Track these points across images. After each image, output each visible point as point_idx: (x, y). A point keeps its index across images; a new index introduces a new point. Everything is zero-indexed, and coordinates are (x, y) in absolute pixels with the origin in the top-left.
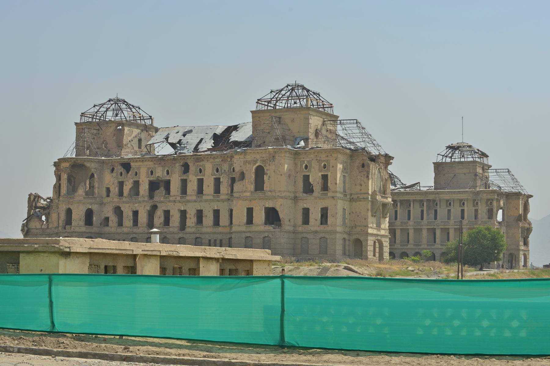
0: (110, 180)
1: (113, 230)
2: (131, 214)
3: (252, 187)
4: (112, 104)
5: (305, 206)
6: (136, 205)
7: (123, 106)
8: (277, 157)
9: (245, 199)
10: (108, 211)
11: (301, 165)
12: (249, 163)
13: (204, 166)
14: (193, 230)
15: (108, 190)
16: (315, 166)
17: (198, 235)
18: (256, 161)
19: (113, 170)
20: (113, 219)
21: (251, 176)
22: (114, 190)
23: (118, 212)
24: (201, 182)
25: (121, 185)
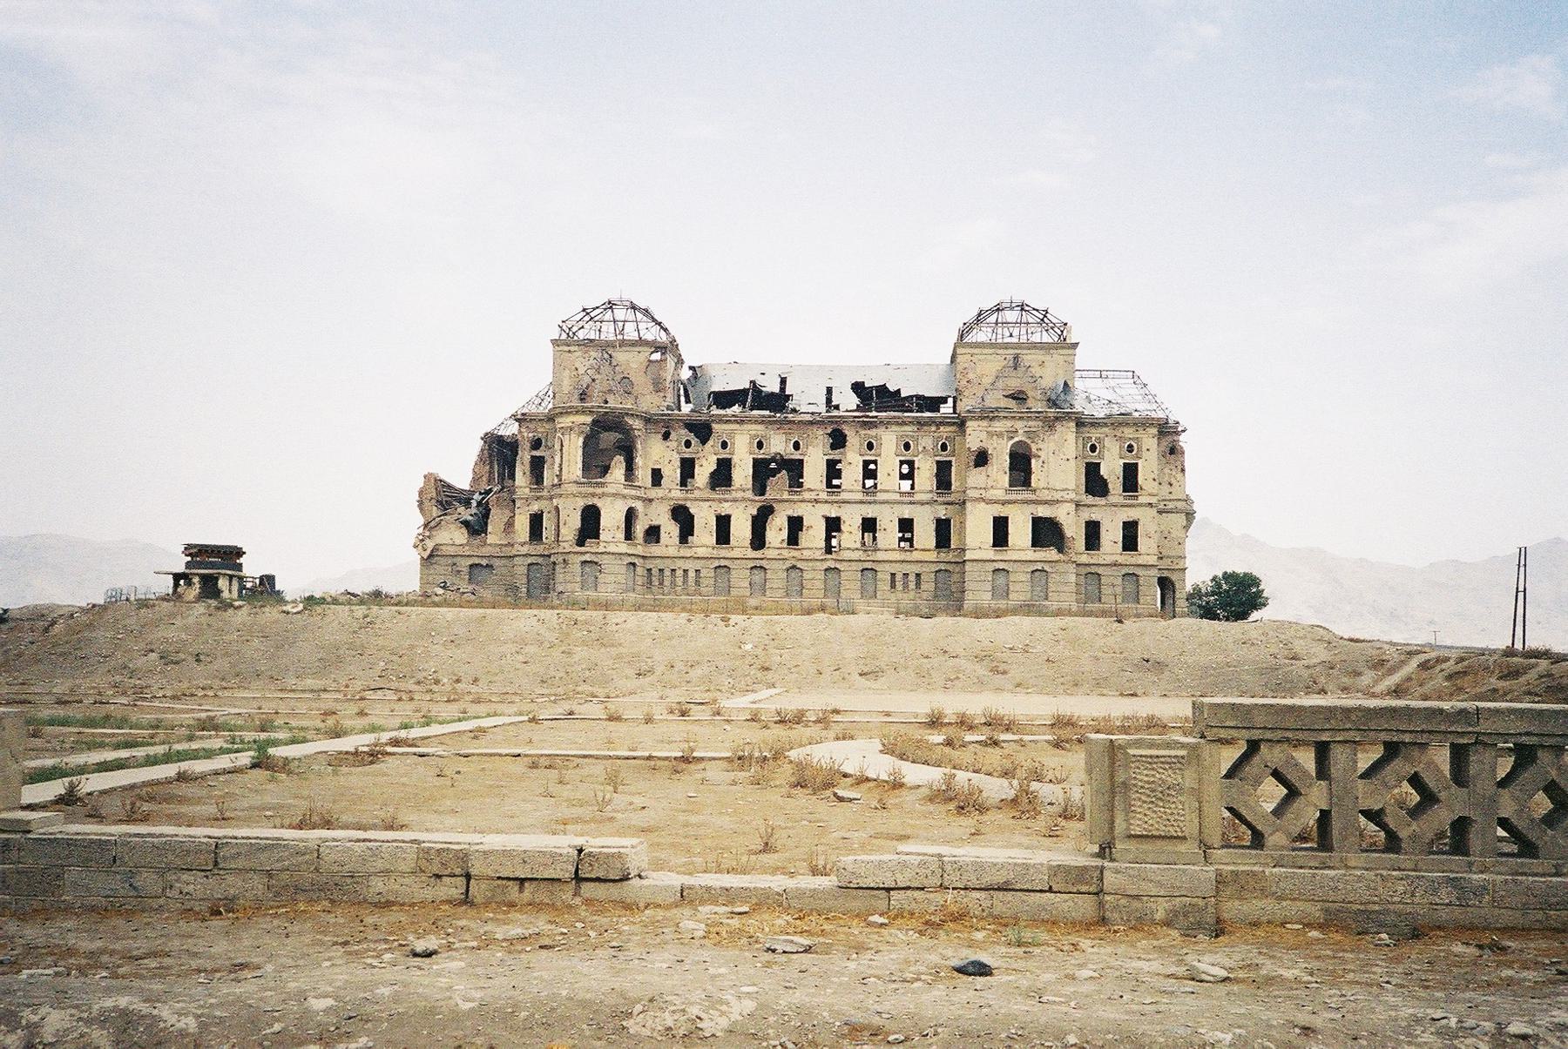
1: (672, 551)
5: (1094, 517)
12: (1000, 435)
19: (666, 436)
20: (670, 530)
22: (672, 473)
23: (683, 518)
25: (688, 468)
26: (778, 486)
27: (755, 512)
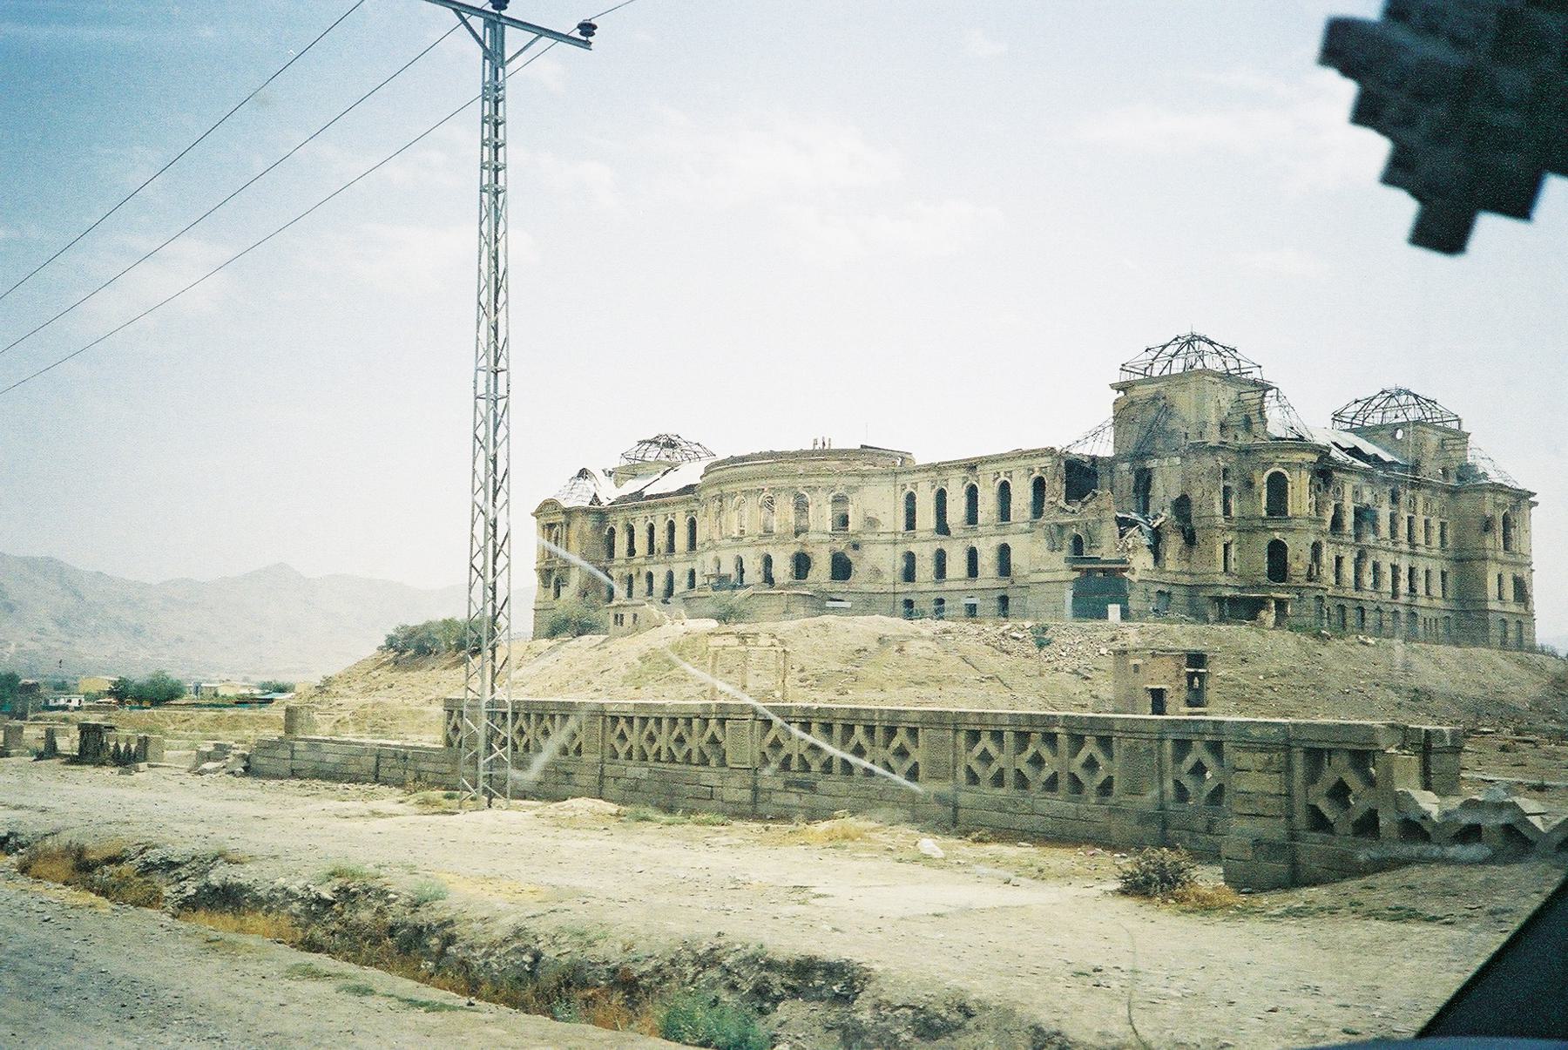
26: (1366, 526)
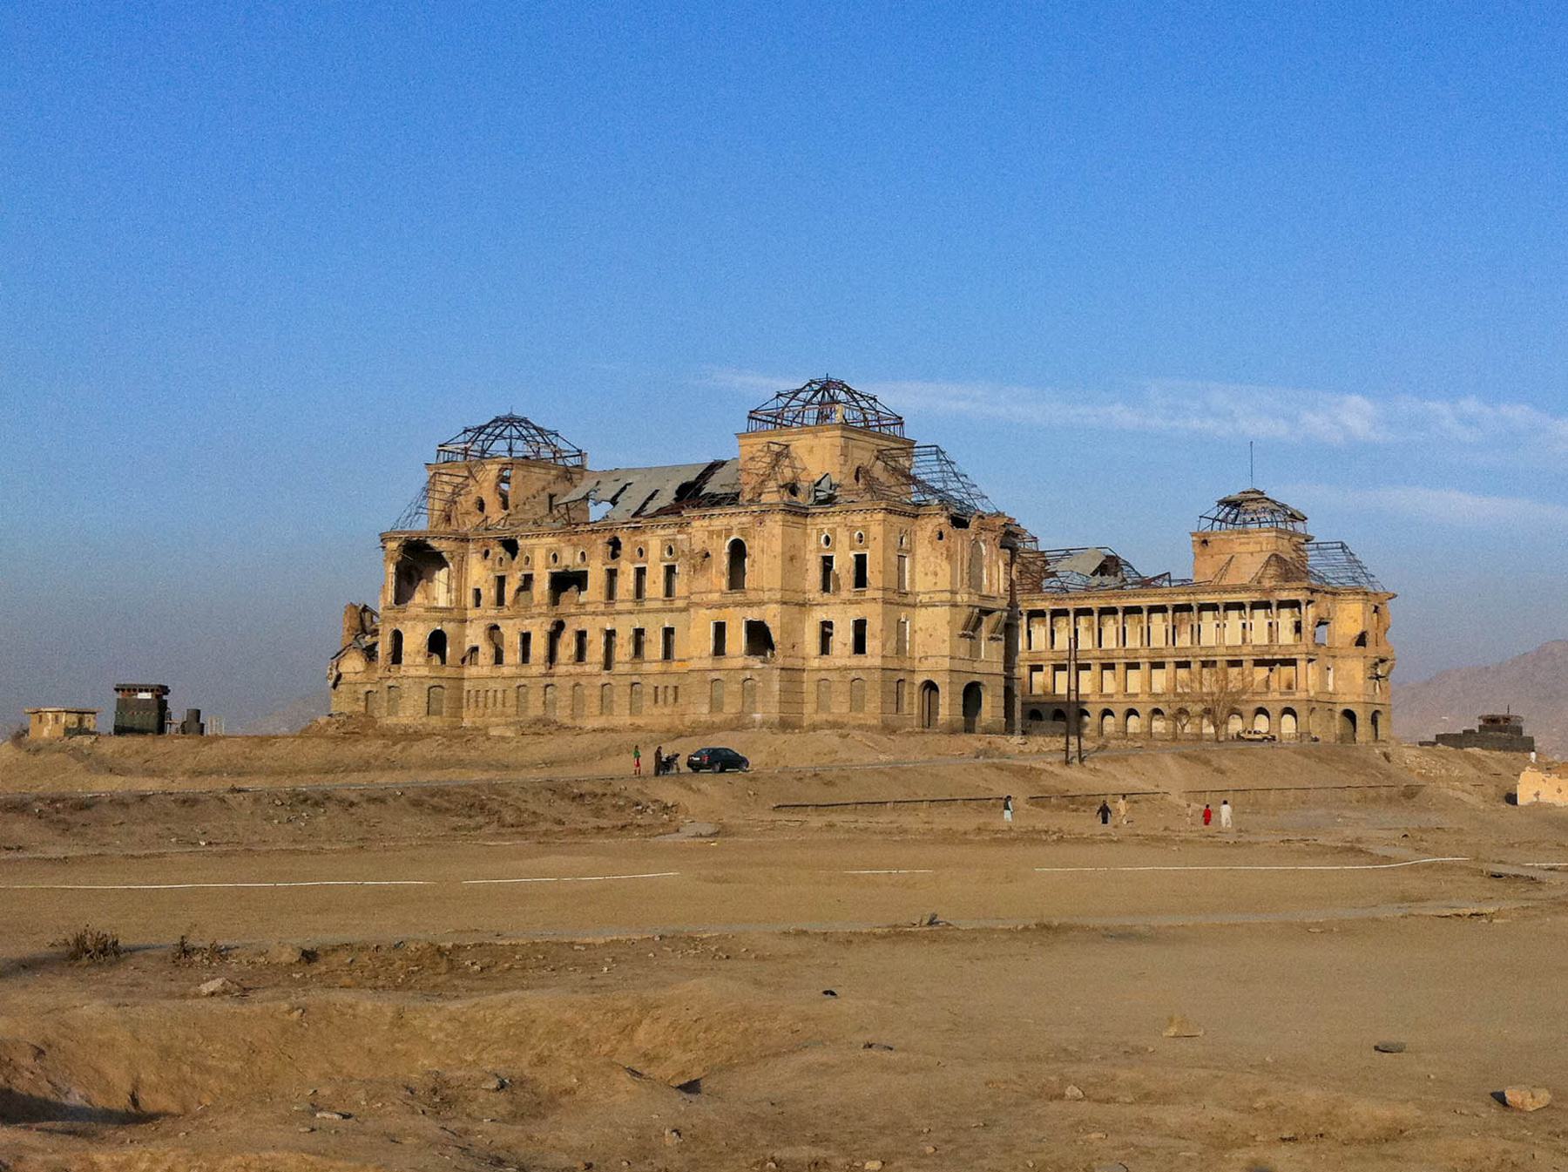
0: (479, 573)
2: (518, 639)
3: (724, 583)
4: (817, 392)
6: (527, 622)
7: (842, 396)
8: (768, 522)
9: (710, 606)
10: (475, 635)
11: (818, 539)
13: (646, 543)
14: (627, 668)
15: (477, 593)
16: (842, 538)
17: (635, 679)
18: (729, 532)
20: (486, 651)
21: (722, 559)
22: (489, 594)
24: (641, 572)
25: (501, 581)
26: (570, 597)
27: (548, 628)
